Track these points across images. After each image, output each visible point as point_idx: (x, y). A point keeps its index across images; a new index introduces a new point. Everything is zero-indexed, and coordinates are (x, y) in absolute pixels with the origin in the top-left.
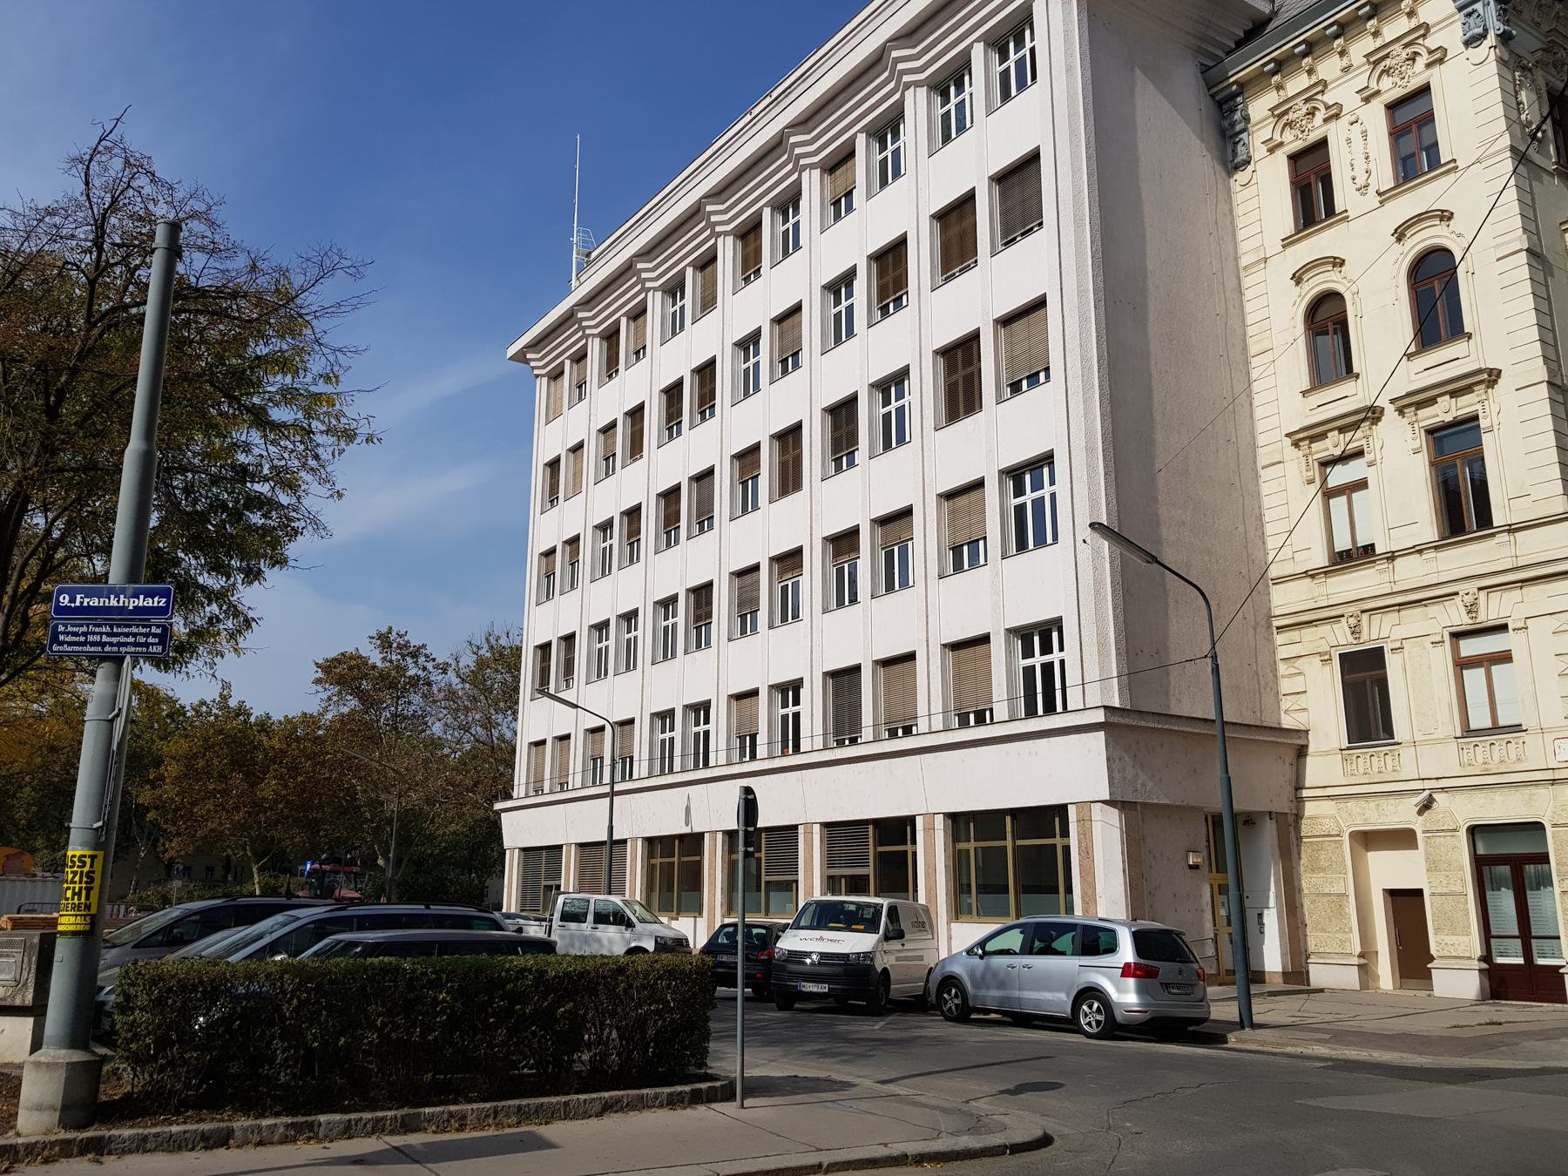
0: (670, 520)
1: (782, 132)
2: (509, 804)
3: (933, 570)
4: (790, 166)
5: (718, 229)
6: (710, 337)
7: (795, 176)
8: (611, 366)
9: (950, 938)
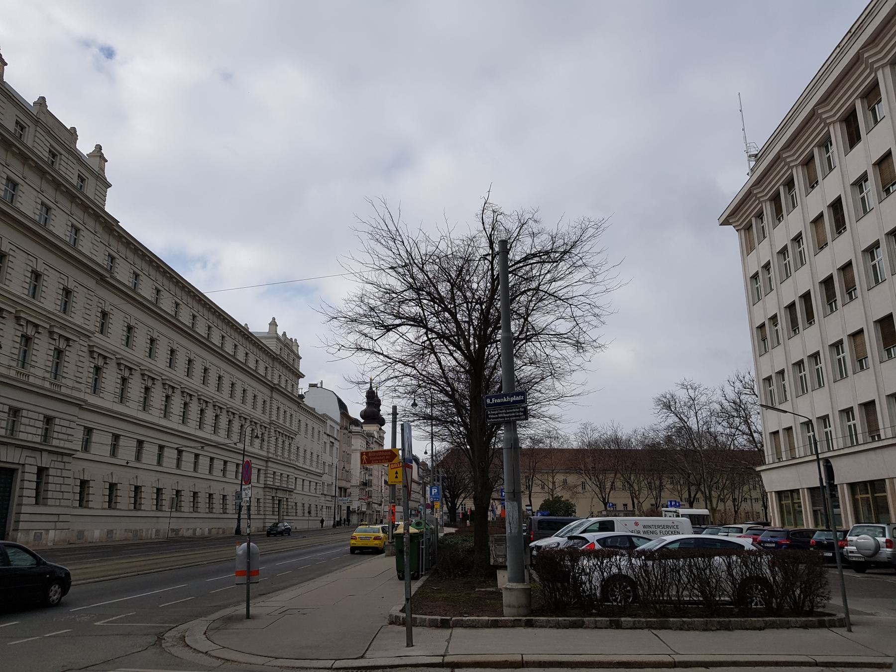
0: (830, 297)
1: (858, 52)
2: (764, 467)
3: (877, 359)
4: (868, 71)
5: (792, 165)
6: (832, 186)
7: (873, 75)
8: (778, 214)
9: (13, 463)
